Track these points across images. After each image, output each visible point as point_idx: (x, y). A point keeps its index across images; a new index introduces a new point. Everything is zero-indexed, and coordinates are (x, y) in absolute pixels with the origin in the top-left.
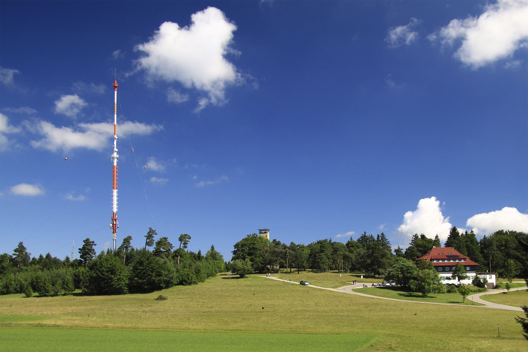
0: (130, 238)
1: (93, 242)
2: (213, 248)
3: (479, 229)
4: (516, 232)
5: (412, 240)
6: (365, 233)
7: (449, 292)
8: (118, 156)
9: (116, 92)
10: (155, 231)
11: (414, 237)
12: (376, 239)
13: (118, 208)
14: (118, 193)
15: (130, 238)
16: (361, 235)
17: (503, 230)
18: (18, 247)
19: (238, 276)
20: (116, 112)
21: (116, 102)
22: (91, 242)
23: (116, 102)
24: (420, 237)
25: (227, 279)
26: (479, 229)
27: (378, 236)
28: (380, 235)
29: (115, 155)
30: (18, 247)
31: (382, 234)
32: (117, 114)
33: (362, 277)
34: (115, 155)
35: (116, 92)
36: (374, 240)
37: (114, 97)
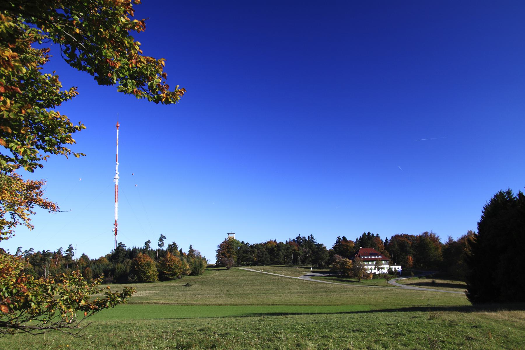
0: (149, 242)
1: (124, 245)
2: (387, 238)
3: (378, 279)
4: (408, 235)
5: (337, 241)
6: (299, 235)
7: (373, 278)
8: (119, 178)
9: (118, 130)
10: (165, 236)
11: (338, 239)
12: (307, 240)
13: (119, 217)
14: (119, 205)
15: (149, 242)
16: (297, 237)
17: (509, 193)
18: (285, 243)
19: (226, 268)
20: (118, 145)
21: (118, 137)
22: (122, 245)
23: (118, 137)
24: (342, 238)
25: (260, 262)
26: (378, 279)
27: (309, 236)
28: (310, 236)
29: (117, 176)
30: (285, 243)
31: (312, 236)
32: (118, 146)
33: (312, 268)
34: (117, 176)
35: (118, 130)
36: (306, 240)
37: (117, 134)
